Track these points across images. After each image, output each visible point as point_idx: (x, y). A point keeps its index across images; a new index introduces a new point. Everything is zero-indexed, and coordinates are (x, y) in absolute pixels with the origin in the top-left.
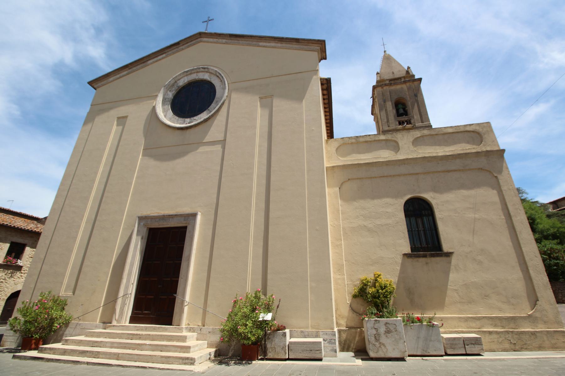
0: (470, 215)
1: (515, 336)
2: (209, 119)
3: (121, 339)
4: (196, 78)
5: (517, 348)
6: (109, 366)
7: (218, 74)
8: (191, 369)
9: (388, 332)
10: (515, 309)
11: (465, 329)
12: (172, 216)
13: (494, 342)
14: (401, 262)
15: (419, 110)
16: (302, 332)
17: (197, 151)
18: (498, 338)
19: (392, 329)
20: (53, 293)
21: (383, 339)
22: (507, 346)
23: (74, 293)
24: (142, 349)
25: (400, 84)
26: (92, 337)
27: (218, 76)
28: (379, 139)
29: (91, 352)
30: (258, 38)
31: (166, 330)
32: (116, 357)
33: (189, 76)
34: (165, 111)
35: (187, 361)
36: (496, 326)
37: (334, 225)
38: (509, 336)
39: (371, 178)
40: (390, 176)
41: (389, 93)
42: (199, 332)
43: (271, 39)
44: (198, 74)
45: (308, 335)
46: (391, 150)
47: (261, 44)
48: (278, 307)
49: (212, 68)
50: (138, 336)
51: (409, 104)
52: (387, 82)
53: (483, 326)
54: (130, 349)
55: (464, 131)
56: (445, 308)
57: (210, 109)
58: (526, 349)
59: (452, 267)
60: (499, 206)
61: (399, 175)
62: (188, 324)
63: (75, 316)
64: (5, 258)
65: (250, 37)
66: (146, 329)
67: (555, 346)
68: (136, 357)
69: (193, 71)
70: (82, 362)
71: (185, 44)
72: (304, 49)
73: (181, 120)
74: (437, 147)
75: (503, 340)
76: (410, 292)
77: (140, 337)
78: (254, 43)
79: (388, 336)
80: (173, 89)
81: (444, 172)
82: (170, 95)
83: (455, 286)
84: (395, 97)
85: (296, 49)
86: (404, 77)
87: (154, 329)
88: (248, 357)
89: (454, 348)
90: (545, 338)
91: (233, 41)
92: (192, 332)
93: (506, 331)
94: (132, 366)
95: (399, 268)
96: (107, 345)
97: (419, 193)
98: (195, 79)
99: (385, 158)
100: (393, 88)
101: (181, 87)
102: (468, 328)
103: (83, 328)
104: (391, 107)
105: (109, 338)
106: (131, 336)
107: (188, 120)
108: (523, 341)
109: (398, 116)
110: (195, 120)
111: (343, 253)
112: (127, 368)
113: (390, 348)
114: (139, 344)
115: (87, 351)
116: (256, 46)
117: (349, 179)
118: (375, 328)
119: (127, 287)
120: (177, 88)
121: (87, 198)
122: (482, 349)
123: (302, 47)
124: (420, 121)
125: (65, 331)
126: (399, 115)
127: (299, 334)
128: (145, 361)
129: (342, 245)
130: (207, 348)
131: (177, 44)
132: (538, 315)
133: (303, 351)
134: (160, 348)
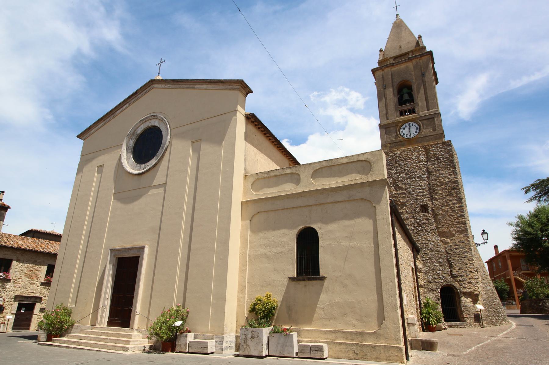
0: (346, 244)
1: (359, 348)
2: (156, 165)
4: (150, 125)
5: (359, 357)
8: (123, 353)
9: (253, 337)
10: (365, 326)
11: (323, 339)
13: (342, 351)
14: (287, 284)
15: (426, 94)
16: (204, 335)
17: (148, 194)
18: (345, 348)
19: (255, 335)
20: (64, 305)
21: (249, 343)
22: (351, 355)
23: (76, 305)
25: (404, 63)
26: (83, 334)
28: (285, 173)
31: (124, 331)
32: (90, 345)
33: (145, 123)
34: (128, 159)
35: (124, 349)
36: (347, 339)
37: (243, 253)
38: (354, 348)
39: (275, 210)
40: (290, 208)
41: (390, 77)
42: (144, 333)
45: (207, 338)
46: (294, 183)
47: (196, 86)
50: (107, 334)
51: (414, 87)
52: (392, 61)
53: (337, 338)
54: (99, 341)
55: (357, 161)
56: (313, 322)
58: (365, 359)
59: (324, 289)
60: (371, 235)
61: (296, 208)
64: (45, 278)
66: (114, 330)
67: (389, 359)
69: (147, 119)
71: (142, 92)
72: (228, 89)
74: (332, 178)
75: (349, 350)
76: (289, 309)
78: (191, 86)
79: (252, 340)
80: (134, 137)
81: (332, 203)
82: (132, 143)
83: (323, 305)
84: (398, 80)
86: (412, 51)
87: (118, 330)
88: (165, 350)
89: (303, 353)
90: (382, 352)
92: (140, 333)
93: (353, 343)
94: (95, 350)
95: (284, 289)
96: (88, 339)
97: (310, 224)
98: (149, 126)
99: (287, 191)
100: (395, 69)
101: (139, 135)
102: (326, 339)
104: (392, 94)
108: (364, 352)
109: (400, 105)
111: (247, 276)
113: (252, 348)
115: (76, 342)
116: (192, 89)
117: (258, 212)
118: (245, 335)
119: (104, 301)
122: (323, 355)
124: (426, 109)
125: (71, 330)
126: (401, 102)
127: (202, 337)
128: (104, 348)
129: (246, 270)
131: (135, 94)
132: (381, 332)
133: (197, 347)
134: (114, 341)
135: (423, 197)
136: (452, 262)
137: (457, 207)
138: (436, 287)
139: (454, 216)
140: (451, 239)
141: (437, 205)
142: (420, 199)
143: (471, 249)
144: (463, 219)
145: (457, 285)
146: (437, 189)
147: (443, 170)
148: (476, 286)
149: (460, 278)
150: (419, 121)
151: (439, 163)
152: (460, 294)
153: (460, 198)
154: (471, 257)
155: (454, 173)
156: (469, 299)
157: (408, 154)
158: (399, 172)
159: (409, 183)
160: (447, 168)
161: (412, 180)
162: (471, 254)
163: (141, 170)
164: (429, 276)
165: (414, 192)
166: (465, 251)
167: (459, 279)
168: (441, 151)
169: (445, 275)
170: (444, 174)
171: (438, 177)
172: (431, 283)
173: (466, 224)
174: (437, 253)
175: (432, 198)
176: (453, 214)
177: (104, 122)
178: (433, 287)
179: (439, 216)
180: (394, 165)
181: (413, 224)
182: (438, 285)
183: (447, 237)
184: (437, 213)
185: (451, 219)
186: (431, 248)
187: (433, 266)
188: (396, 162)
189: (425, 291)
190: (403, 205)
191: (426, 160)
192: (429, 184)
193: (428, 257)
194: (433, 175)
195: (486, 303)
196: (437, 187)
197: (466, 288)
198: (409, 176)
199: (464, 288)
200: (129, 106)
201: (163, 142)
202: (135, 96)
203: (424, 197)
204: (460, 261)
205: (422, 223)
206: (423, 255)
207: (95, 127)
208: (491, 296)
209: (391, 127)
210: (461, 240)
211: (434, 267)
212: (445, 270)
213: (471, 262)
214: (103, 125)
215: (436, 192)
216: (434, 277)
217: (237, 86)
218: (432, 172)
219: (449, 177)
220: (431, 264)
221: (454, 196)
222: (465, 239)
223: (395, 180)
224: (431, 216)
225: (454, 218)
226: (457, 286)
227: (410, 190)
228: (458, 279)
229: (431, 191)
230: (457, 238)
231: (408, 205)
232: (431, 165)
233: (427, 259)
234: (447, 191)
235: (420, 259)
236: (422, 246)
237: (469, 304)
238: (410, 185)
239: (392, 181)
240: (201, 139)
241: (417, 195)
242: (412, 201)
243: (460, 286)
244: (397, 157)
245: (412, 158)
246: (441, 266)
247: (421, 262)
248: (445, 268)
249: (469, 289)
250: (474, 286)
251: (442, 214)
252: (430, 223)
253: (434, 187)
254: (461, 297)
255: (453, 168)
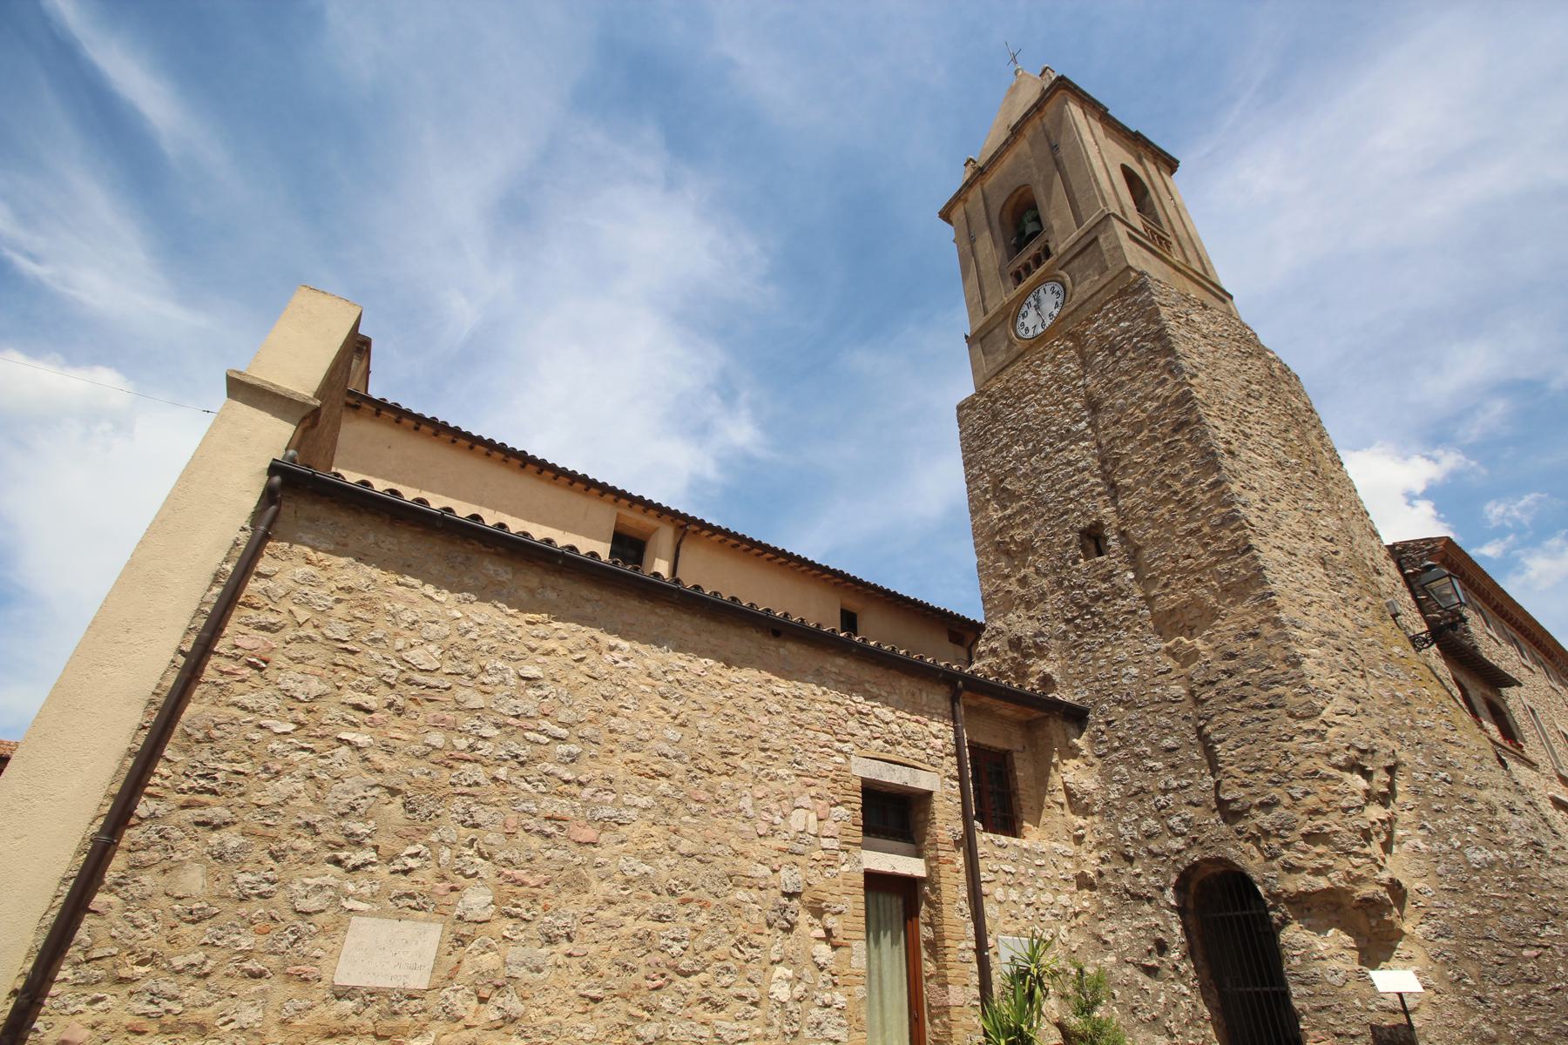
135: (1082, 500)
136: (1214, 742)
137: (1204, 492)
138: (1152, 879)
139: (1199, 529)
140: (1207, 633)
141: (1132, 509)
142: (1073, 511)
143: (1294, 656)
144: (1233, 531)
145: (1251, 861)
146: (1124, 452)
147: (1133, 379)
148: (1357, 855)
149: (1263, 815)
150: (1060, 269)
151: (1117, 362)
152: (1274, 908)
153: (1208, 454)
154: (1302, 700)
155: (1171, 372)
156: (1331, 932)
157: (1026, 376)
158: (1006, 444)
159: (1036, 468)
160: (1147, 363)
161: (1043, 455)
162: (1300, 681)
164: (1124, 825)
165: (1053, 495)
166: (1268, 672)
167: (1257, 821)
168: (1120, 320)
169: (1189, 813)
170: (1139, 389)
171: (1122, 410)
172: (1130, 860)
173: (1250, 548)
174: (1156, 707)
175: (1114, 491)
176: (1193, 525)
178: (1142, 880)
179: (1146, 553)
180: (990, 429)
181: (1062, 609)
182: (1163, 869)
183: (1191, 629)
184: (1138, 539)
185: (1189, 549)
186: (1128, 694)
187: (1140, 775)
188: (995, 416)
189: (1102, 907)
190: (1025, 550)
191: (1081, 372)
192: (1099, 445)
193: (1120, 734)
194: (1106, 411)
195: (1458, 947)
196: (1123, 446)
197: (1300, 869)
198: (1034, 446)
199: (1291, 869)
203: (1087, 498)
204: (1250, 726)
205: (1092, 599)
206: (1099, 730)
208: (1502, 904)
209: (994, 328)
210: (1244, 628)
211: (1144, 778)
212: (1190, 784)
213: (1306, 726)
215: (1122, 464)
216: (1144, 827)
218: (1100, 401)
219: (1159, 391)
220: (1130, 766)
221: (1189, 453)
222: (1263, 617)
223: (997, 476)
224: (1122, 558)
225: (1199, 539)
226: (1251, 864)
227: (1041, 489)
228: (1250, 822)
229: (1106, 467)
230: (1227, 624)
231: (1040, 546)
232: (1095, 382)
233: (1116, 744)
234: (1157, 444)
235: (1085, 752)
236: (1097, 691)
237: (1335, 964)
238: (1040, 473)
239: (989, 482)
241: (1065, 500)
242: (1049, 525)
243: (1267, 859)
244: (996, 400)
245: (1039, 385)
246: (1173, 766)
247: (1092, 765)
248: (1191, 775)
249: (1317, 872)
250: (1349, 853)
251: (1155, 540)
252: (1119, 588)
253: (1112, 448)
254: (1280, 928)
255: (1167, 356)
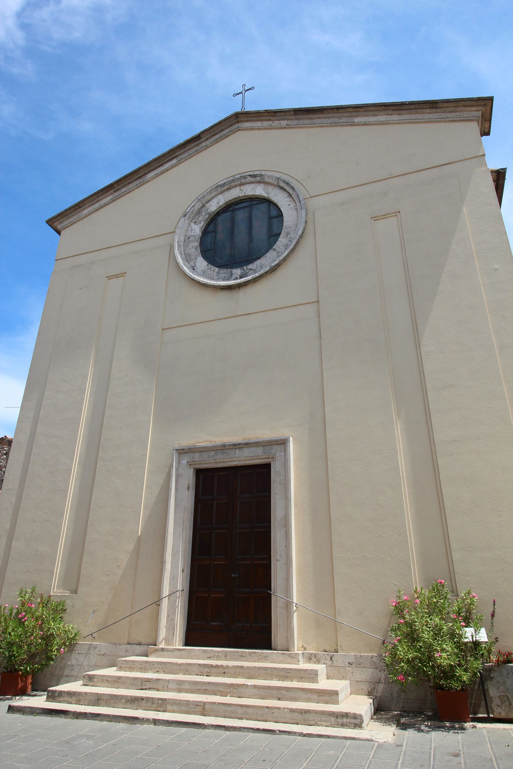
3: (187, 674)
4: (241, 195)
6: (197, 727)
7: (282, 184)
12: (240, 446)
24: (240, 696)
27: (282, 188)
29: (148, 699)
30: (351, 110)
31: (265, 658)
32: (199, 709)
33: (226, 192)
35: (345, 720)
43: (379, 108)
44: (242, 187)
47: (357, 120)
48: (493, 615)
49: (269, 173)
50: (221, 670)
54: (216, 695)
57: (277, 249)
62: (303, 646)
63: (85, 632)
65: (336, 111)
68: (240, 710)
70: (143, 718)
73: (224, 273)
77: (224, 671)
78: (344, 120)
80: (201, 218)
85: (430, 122)
91: (301, 122)
98: (239, 197)
103: (103, 653)
105: (164, 672)
106: (207, 669)
107: (237, 272)
110: (250, 270)
112: (234, 732)
114: (232, 685)
115: (142, 699)
120: (207, 216)
121: (76, 422)
123: (443, 115)
128: (259, 718)
130: (351, 694)
134: (275, 692)
163: (234, 280)
177: (117, 194)
200: (179, 164)
201: (284, 224)
202: (193, 145)
207: (92, 205)
214: (113, 201)
217: (473, 113)
240: (126, 273)
